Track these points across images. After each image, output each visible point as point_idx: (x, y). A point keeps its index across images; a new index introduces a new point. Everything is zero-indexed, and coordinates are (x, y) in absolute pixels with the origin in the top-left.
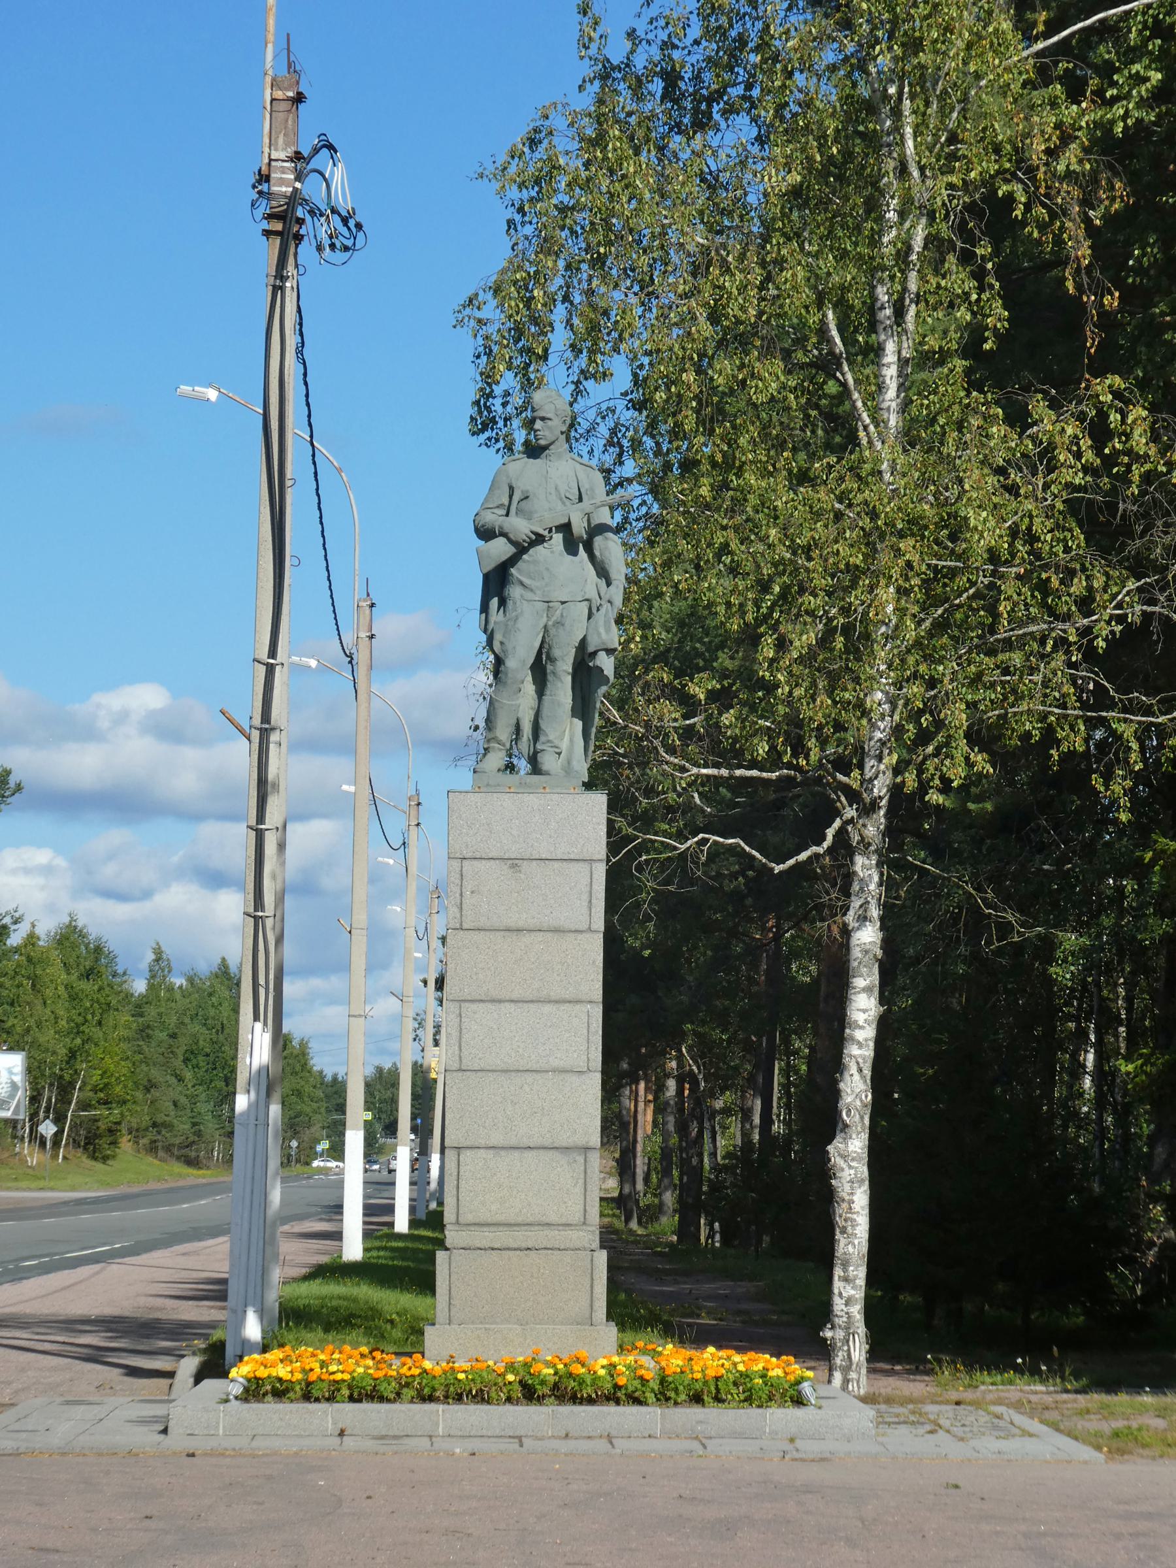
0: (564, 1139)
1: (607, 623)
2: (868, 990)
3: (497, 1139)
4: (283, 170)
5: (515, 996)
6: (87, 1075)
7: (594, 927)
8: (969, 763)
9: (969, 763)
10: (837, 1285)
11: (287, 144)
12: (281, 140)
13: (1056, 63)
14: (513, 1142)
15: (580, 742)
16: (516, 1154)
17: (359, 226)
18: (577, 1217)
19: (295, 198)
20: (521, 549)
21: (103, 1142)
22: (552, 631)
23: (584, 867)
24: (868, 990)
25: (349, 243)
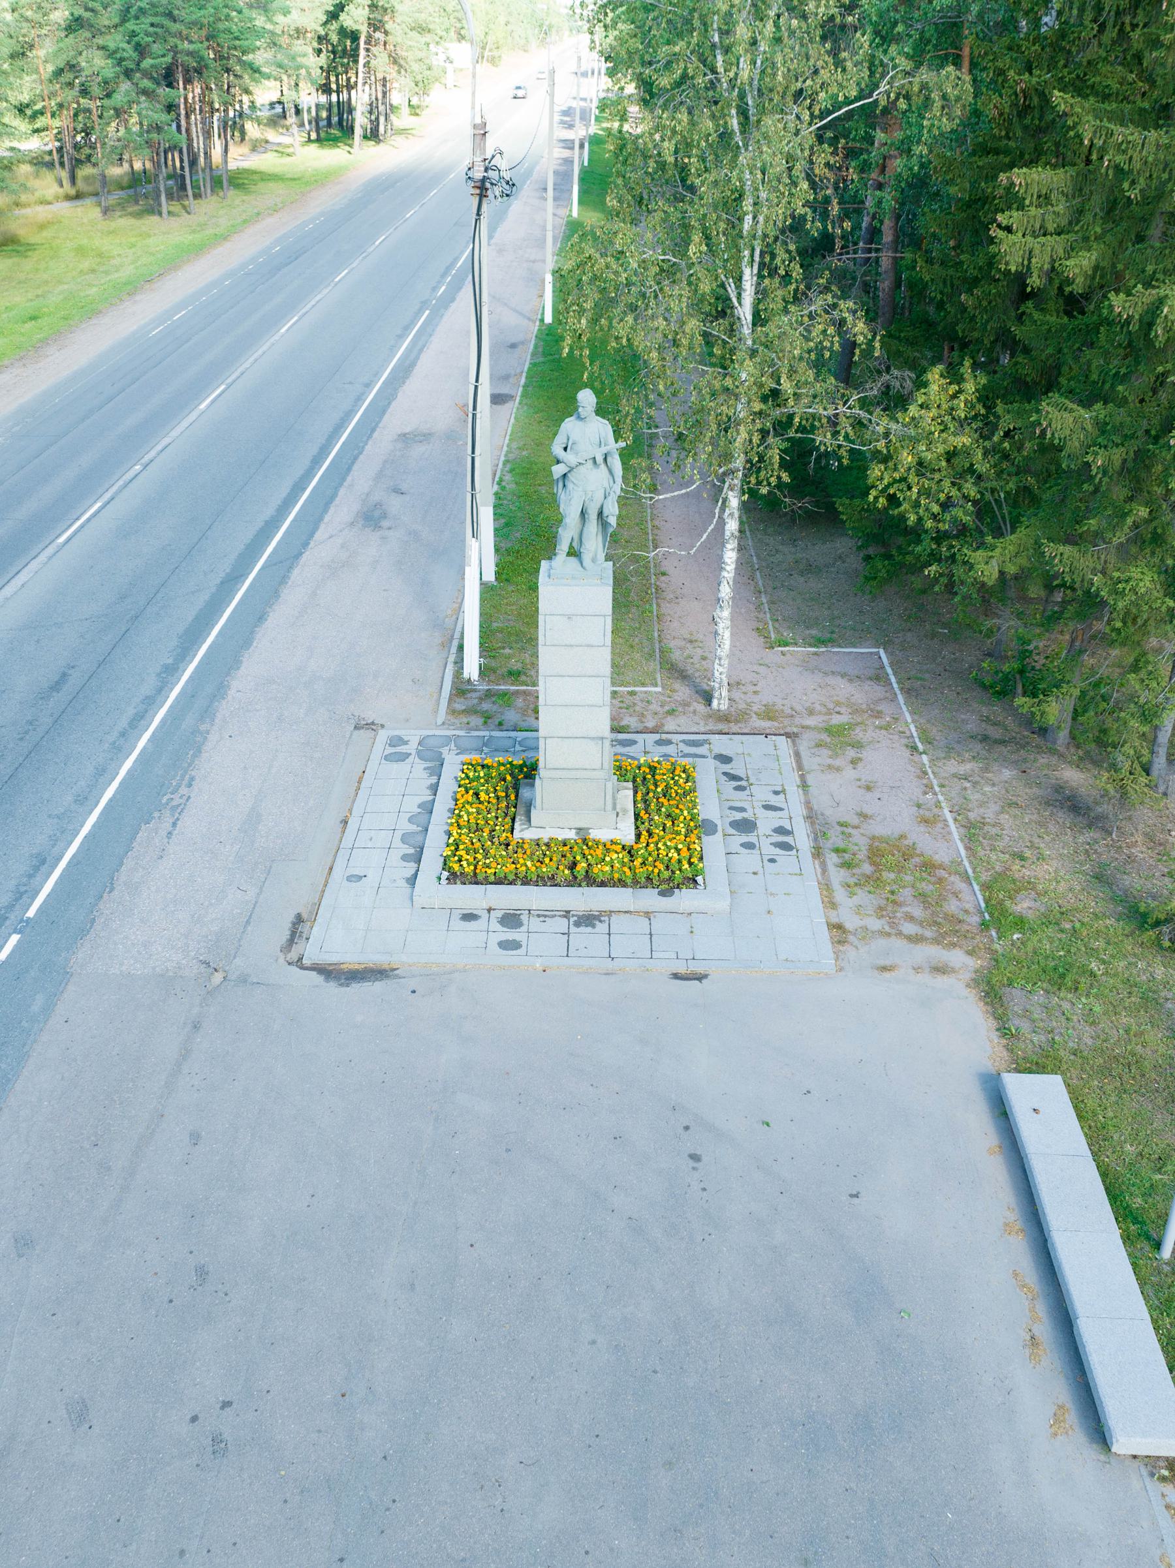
0: (593, 734)
1: (613, 503)
2: (733, 549)
3: (562, 734)
4: (479, 166)
5: (570, 674)
6: (491, 39)
7: (606, 703)
8: (779, 478)
9: (779, 478)
10: (716, 666)
11: (481, 154)
12: (478, 152)
13: (825, 133)
14: (570, 735)
15: (601, 545)
16: (571, 740)
17: (514, 185)
18: (598, 766)
19: (484, 180)
20: (571, 469)
21: (496, 60)
22: (587, 502)
23: (602, 619)
24: (733, 549)
25: (508, 192)
